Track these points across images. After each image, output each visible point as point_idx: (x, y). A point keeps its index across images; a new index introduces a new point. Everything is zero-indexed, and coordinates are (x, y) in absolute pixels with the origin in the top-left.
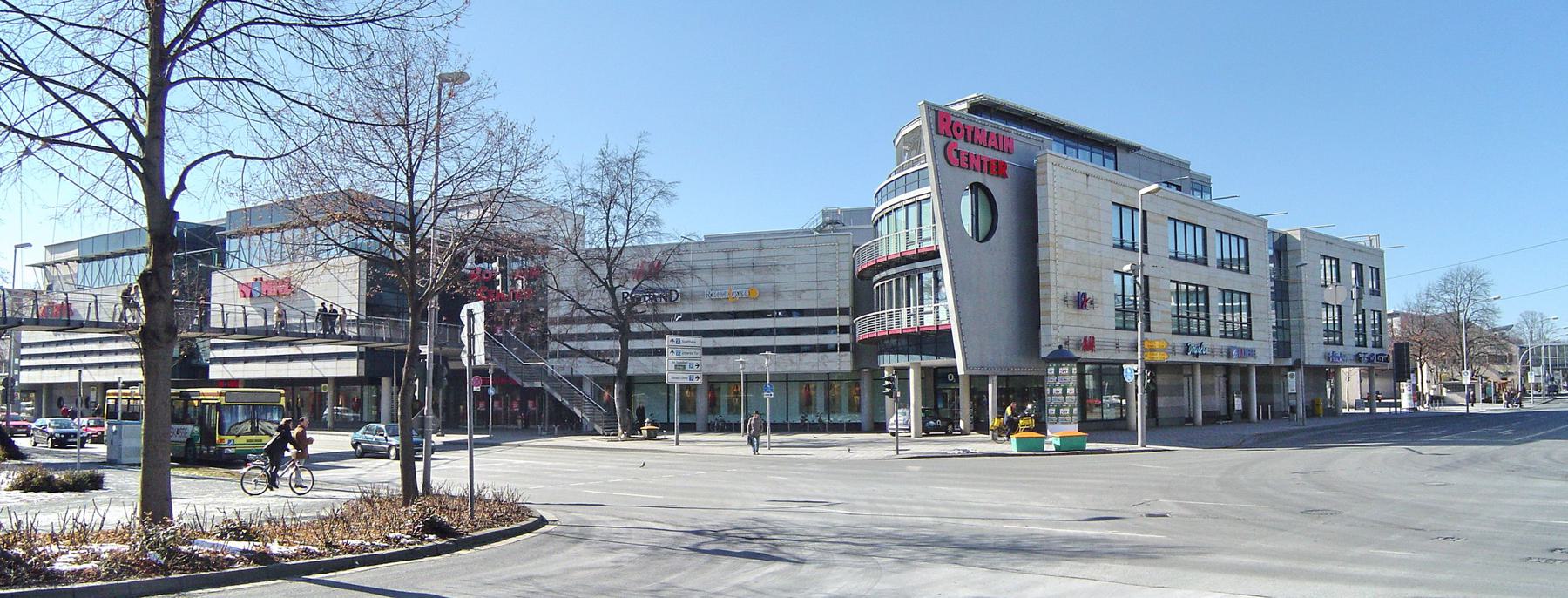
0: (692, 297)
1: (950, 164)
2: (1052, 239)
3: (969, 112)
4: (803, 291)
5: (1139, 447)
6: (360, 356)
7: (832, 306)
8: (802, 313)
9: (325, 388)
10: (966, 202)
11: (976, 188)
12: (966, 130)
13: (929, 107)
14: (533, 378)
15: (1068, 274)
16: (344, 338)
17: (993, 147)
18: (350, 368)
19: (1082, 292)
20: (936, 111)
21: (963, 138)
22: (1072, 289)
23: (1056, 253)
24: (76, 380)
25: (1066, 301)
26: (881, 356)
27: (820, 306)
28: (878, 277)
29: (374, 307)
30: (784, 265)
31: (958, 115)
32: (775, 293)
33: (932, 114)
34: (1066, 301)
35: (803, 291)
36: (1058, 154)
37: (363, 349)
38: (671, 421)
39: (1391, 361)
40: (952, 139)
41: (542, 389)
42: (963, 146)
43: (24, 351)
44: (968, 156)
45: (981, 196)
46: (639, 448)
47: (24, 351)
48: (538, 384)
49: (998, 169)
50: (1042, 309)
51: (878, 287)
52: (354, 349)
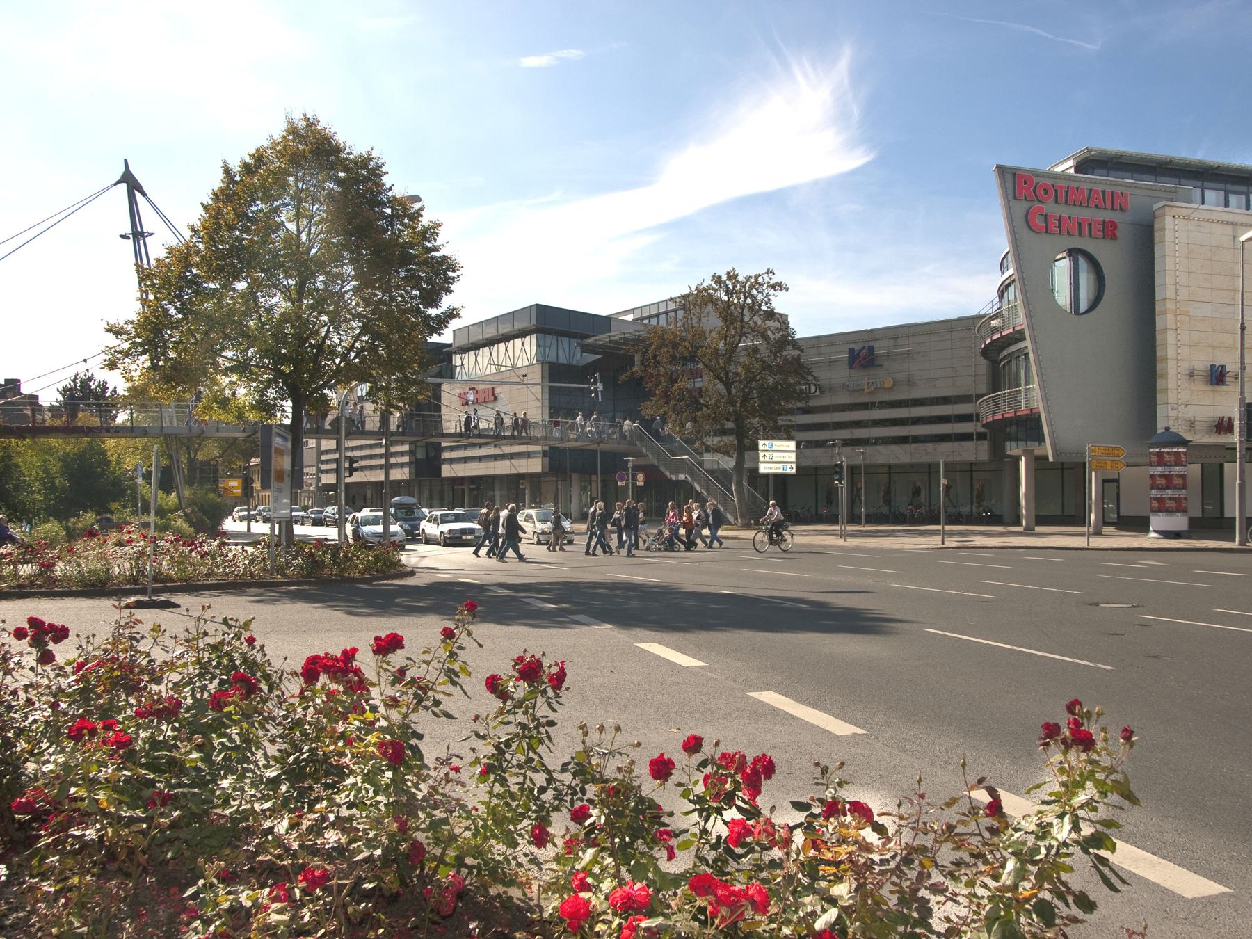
0: (831, 389)
1: (1031, 229)
2: (1170, 306)
3: (1076, 171)
4: (938, 379)
5: (1235, 544)
6: (545, 454)
7: (967, 393)
8: (946, 400)
9: (523, 484)
10: (1063, 267)
11: (1073, 253)
12: (1056, 191)
13: (1002, 170)
14: (677, 472)
15: (1197, 345)
16: (531, 440)
17: (1097, 206)
18: (534, 466)
19: (1217, 364)
20: (1015, 174)
21: (1053, 198)
22: (1202, 361)
23: (1177, 321)
24: (382, 478)
25: (1191, 376)
26: (1008, 443)
27: (955, 393)
28: (1005, 353)
29: (554, 410)
30: (918, 353)
31: (1063, 176)
32: (910, 382)
33: (1009, 178)
34: (1191, 376)
35: (938, 379)
36: (1238, 211)
37: (547, 448)
38: (1227, 515)
39: (1236, 429)
40: (1036, 202)
41: (685, 482)
42: (1050, 208)
43: (324, 457)
44: (1059, 220)
45: (1083, 263)
46: (1115, 546)
47: (324, 457)
48: (682, 477)
49: (1110, 230)
50: (1159, 387)
51: (1004, 366)
52: (538, 448)
